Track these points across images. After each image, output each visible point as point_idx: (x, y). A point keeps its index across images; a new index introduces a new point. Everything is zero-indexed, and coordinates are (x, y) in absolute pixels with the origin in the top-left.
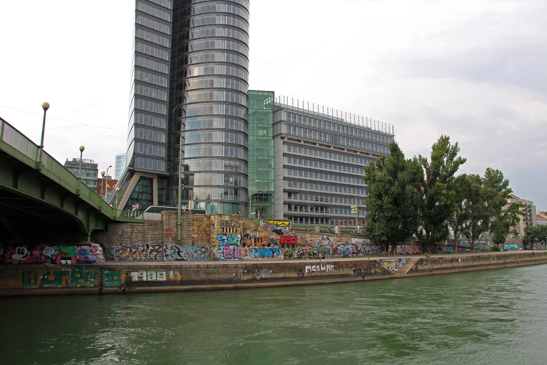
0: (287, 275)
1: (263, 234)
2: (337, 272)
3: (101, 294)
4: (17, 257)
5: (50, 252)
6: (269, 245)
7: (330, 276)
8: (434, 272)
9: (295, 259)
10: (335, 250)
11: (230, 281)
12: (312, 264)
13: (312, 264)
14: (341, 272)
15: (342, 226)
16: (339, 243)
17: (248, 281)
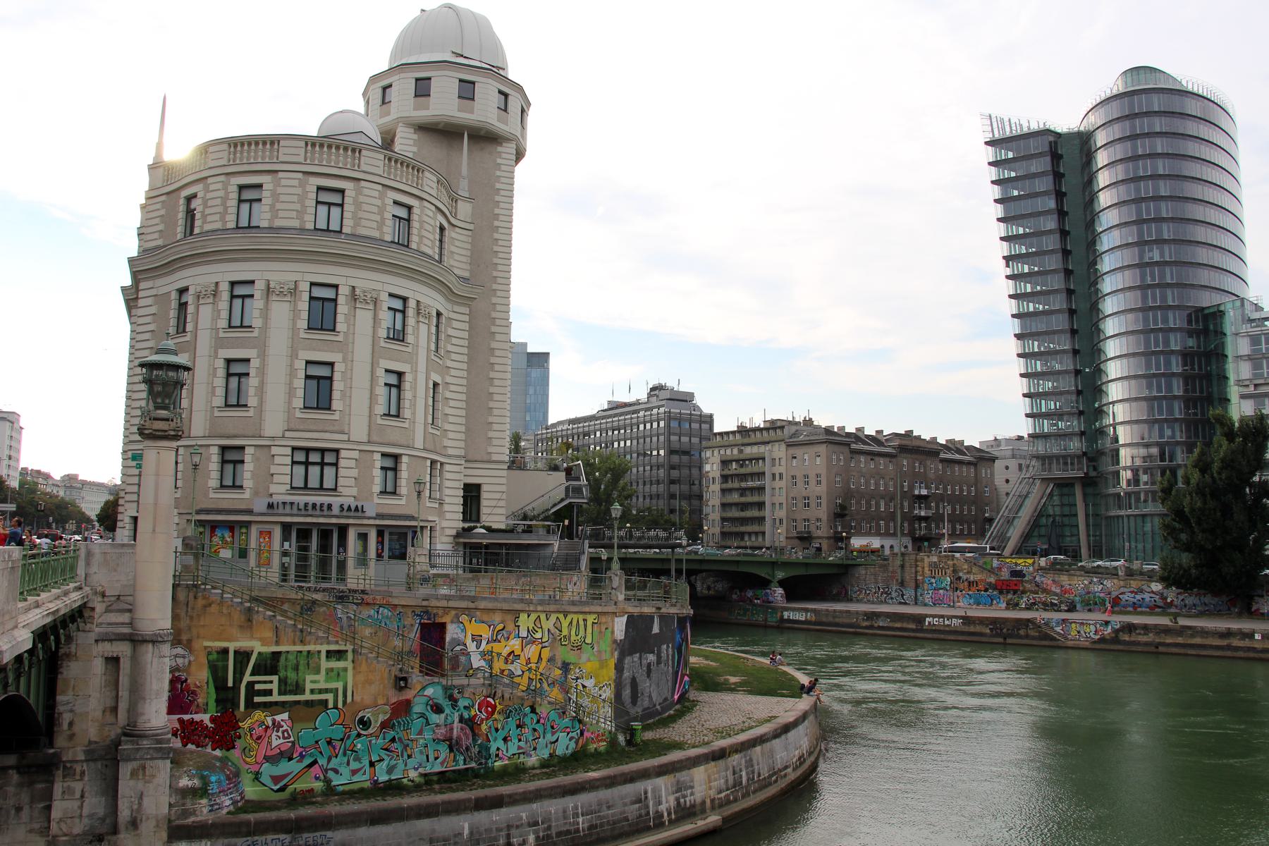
0: (905, 625)
1: (978, 577)
2: (966, 629)
3: (766, 627)
4: (735, 597)
5: (750, 594)
6: (986, 590)
7: (955, 632)
8: (1161, 649)
9: (1021, 609)
10: (1116, 601)
11: (851, 626)
12: (934, 616)
13: (934, 616)
14: (972, 629)
15: (283, 457)
16: (1122, 590)
17: (867, 627)
